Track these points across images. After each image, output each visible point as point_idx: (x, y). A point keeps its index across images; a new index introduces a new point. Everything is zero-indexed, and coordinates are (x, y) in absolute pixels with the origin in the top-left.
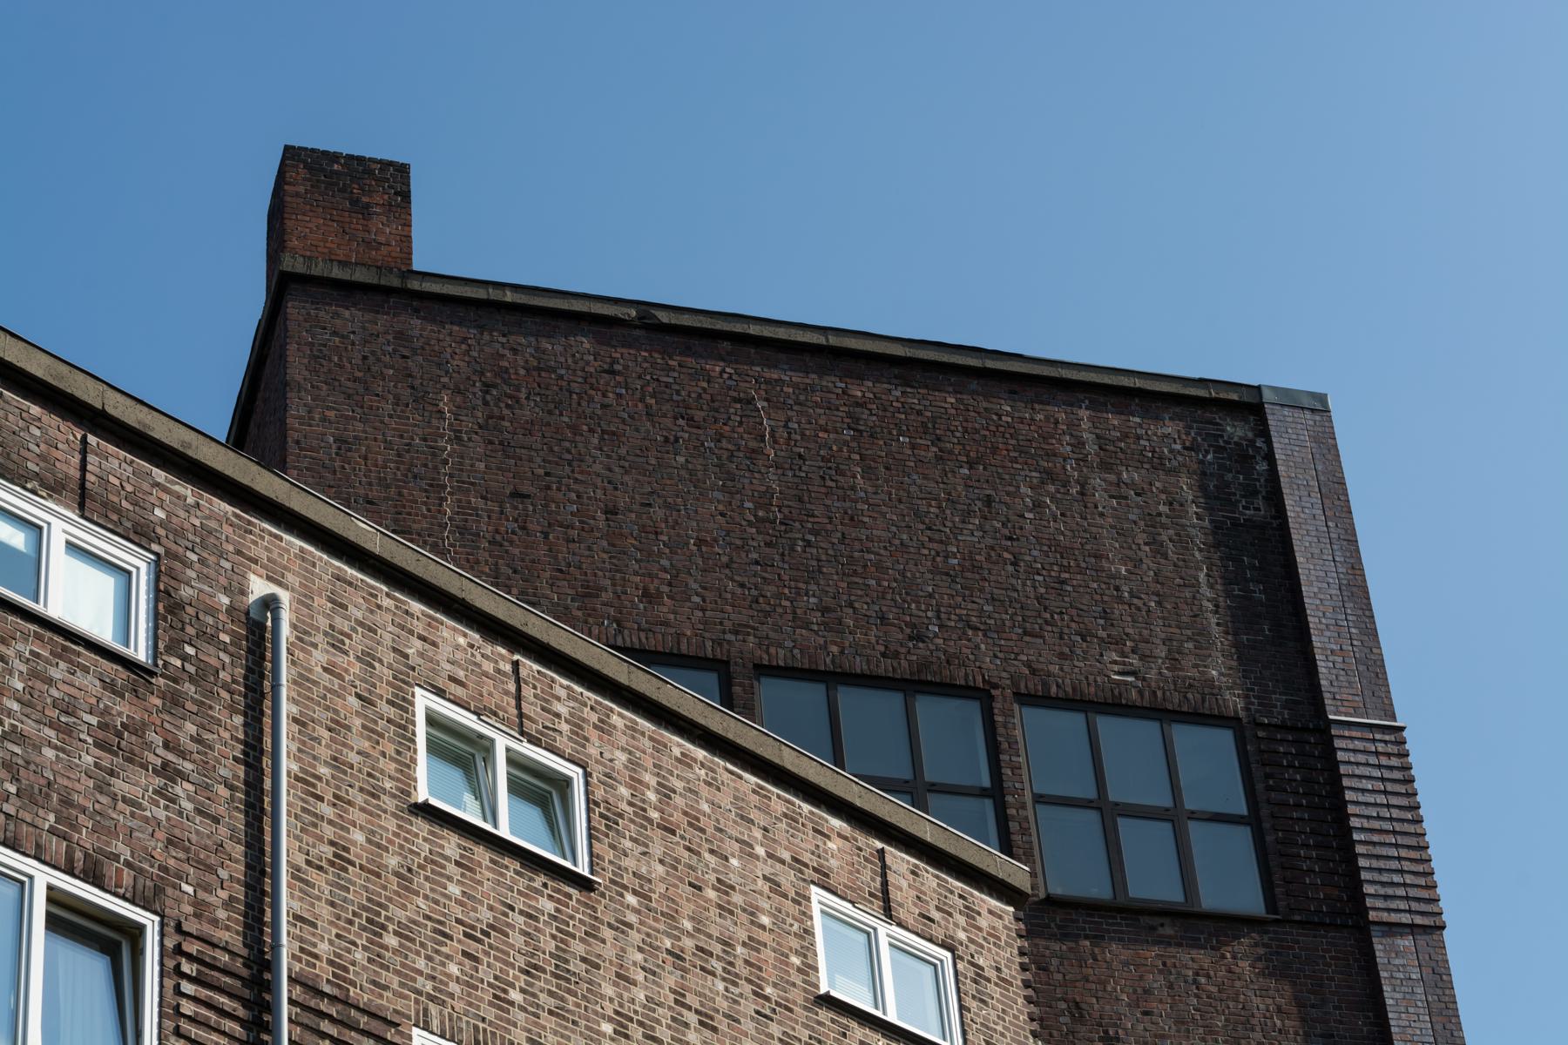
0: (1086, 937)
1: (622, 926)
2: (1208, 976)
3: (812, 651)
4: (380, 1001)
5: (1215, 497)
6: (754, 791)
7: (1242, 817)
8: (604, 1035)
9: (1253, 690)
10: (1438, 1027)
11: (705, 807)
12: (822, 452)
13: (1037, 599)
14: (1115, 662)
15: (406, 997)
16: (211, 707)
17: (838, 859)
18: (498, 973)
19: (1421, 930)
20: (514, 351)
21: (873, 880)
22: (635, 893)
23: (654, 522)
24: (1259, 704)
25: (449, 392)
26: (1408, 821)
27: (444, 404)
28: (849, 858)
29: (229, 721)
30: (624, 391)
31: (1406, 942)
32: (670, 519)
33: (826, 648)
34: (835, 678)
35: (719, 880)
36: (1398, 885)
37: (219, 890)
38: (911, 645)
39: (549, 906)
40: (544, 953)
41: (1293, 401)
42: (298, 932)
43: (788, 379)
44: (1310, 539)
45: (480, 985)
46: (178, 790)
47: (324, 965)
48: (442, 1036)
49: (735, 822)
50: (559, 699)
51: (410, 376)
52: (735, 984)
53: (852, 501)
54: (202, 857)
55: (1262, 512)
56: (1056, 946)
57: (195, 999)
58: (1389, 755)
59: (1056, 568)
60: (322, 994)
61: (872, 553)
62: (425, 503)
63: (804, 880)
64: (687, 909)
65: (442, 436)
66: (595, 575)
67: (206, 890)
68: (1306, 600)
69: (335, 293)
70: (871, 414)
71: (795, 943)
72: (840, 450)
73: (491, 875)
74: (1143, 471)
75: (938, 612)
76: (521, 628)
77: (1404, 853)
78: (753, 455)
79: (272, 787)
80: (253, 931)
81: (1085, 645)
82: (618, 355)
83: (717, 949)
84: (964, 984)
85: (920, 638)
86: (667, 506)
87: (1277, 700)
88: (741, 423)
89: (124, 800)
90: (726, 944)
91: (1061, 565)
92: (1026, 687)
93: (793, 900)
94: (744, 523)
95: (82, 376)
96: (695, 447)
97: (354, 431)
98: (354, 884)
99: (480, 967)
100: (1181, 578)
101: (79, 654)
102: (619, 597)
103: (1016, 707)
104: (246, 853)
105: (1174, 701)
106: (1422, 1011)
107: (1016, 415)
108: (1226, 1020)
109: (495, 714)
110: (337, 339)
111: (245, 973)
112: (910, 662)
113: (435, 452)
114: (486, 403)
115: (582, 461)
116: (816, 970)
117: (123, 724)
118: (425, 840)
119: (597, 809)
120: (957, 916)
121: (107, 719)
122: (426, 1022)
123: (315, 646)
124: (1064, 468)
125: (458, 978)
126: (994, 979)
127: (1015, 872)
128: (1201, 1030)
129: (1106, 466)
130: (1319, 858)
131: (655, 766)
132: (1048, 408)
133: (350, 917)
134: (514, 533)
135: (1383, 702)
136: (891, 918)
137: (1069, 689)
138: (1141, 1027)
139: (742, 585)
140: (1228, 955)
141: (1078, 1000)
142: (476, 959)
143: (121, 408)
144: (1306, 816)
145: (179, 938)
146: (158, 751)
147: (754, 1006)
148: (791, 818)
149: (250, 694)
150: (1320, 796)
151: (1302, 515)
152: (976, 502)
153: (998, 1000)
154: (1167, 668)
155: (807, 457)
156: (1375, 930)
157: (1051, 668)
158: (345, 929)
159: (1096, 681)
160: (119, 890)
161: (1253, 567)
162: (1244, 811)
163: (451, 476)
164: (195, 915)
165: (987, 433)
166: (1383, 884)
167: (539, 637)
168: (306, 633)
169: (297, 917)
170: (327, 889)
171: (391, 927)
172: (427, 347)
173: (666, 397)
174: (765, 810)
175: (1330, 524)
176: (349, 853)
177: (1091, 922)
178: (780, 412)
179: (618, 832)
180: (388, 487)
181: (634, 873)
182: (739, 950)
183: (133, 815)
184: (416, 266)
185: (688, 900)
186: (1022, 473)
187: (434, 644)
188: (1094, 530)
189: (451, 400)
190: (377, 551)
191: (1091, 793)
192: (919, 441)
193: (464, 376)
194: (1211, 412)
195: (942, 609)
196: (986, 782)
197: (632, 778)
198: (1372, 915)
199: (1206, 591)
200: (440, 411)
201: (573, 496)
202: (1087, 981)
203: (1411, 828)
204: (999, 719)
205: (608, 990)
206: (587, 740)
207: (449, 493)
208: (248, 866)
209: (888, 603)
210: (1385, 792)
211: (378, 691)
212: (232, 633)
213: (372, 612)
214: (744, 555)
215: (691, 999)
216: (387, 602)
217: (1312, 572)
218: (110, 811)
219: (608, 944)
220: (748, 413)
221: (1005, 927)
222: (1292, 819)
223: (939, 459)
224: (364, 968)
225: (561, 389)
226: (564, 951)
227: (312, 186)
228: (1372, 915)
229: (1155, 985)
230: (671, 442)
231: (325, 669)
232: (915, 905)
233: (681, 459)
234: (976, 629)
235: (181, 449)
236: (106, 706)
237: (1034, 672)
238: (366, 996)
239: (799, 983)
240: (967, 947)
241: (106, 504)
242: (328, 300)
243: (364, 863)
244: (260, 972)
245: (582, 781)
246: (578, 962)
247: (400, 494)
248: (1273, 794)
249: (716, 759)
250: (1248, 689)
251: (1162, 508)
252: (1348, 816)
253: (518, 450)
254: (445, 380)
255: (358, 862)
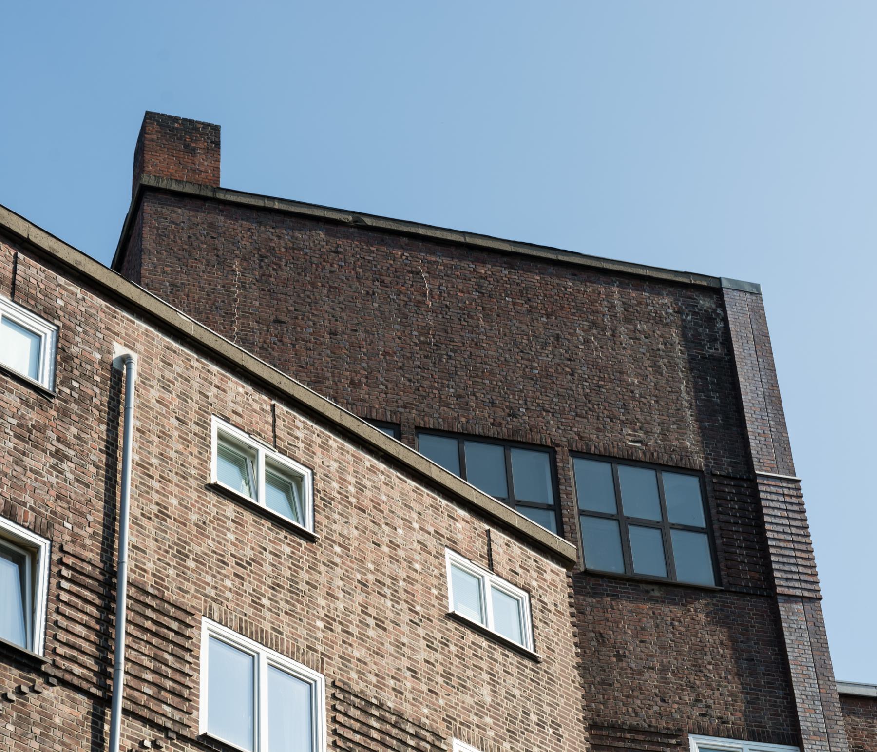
0: (608, 595)
1: (331, 565)
2: (680, 622)
3: (450, 420)
4: (183, 600)
5: (691, 341)
6: (413, 491)
7: (703, 529)
8: (318, 629)
9: (711, 455)
10: (817, 658)
11: (384, 498)
12: (460, 305)
13: (584, 395)
14: (630, 435)
15: (198, 598)
16: (87, 419)
17: (462, 533)
18: (255, 588)
19: (807, 600)
20: (279, 237)
21: (483, 547)
22: (340, 545)
23: (359, 341)
24: (715, 463)
25: (239, 259)
26: (801, 535)
27: (236, 266)
28: (469, 533)
29: (97, 427)
30: (343, 264)
31: (798, 607)
32: (368, 340)
33: (458, 419)
34: (463, 437)
35: (390, 541)
36: (794, 572)
37: (87, 527)
38: (509, 419)
39: (288, 550)
40: (284, 577)
41: (739, 287)
42: (134, 555)
43: (441, 261)
44: (747, 368)
45: (244, 594)
46: (65, 466)
47: (150, 576)
48: (220, 623)
49: (401, 508)
50: (298, 428)
51: (216, 249)
52: (398, 603)
53: (477, 333)
54: (77, 507)
55: (720, 351)
56: (590, 600)
57: (69, 592)
58: (791, 496)
59: (596, 378)
60: (147, 593)
61: (488, 364)
62: (222, 324)
63: (442, 545)
64: (371, 557)
65: (234, 285)
66: (322, 370)
67: (79, 527)
68: (744, 403)
69: (173, 199)
70: (490, 284)
71: (435, 581)
72: (471, 304)
73: (253, 529)
74: (650, 324)
75: (526, 400)
76: (277, 385)
77: (798, 554)
78: (419, 305)
79: (123, 468)
80: (107, 553)
81: (612, 424)
82: (341, 243)
83: (388, 582)
84: (535, 612)
85: (514, 415)
86: (366, 331)
87: (725, 461)
88: (412, 285)
89: (31, 470)
90: (393, 579)
91: (600, 377)
92: (577, 447)
93: (435, 556)
94: (412, 344)
95: (16, 217)
96: (384, 298)
97: (181, 279)
98: (170, 529)
99: (245, 583)
100: (670, 387)
101: (7, 382)
102: (336, 384)
103: (570, 458)
104: (105, 507)
105: (664, 459)
106: (807, 648)
107: (576, 288)
108: (690, 648)
109: (260, 435)
110: (173, 226)
111: (101, 578)
112: (508, 429)
113: (229, 294)
114: (261, 267)
115: (317, 303)
116: (447, 598)
117: (32, 425)
118: (214, 506)
119: (319, 495)
120: (532, 572)
121: (23, 421)
122: (210, 614)
123: (152, 387)
124: (603, 320)
125: (231, 589)
126: (553, 610)
127: (567, 547)
128: (675, 653)
129: (627, 320)
130: (747, 555)
131: (355, 471)
132: (595, 285)
133: (167, 548)
134: (274, 343)
135: (788, 465)
136: (493, 571)
137: (602, 449)
138: (639, 649)
139: (410, 380)
140: (692, 610)
141: (602, 632)
142: (242, 578)
143: (39, 238)
144: (741, 530)
145: (60, 555)
146: (53, 443)
147: (409, 617)
148: (436, 508)
149: (111, 413)
150: (749, 518)
151: (743, 354)
152: (551, 338)
153: (555, 623)
154: (660, 440)
155: (451, 307)
156: (779, 598)
157: (592, 436)
158: (163, 555)
159: (618, 445)
160: (25, 524)
161: (713, 383)
162: (704, 525)
163: (238, 308)
164: (72, 542)
165: (558, 298)
166: (785, 572)
167: (287, 390)
168: (147, 379)
169: (134, 547)
170: (153, 531)
171: (191, 556)
172: (227, 233)
173: (368, 268)
174: (420, 502)
175: (759, 360)
176: (168, 510)
177: (612, 587)
178: (436, 280)
179: (331, 508)
180: (201, 313)
181: (340, 534)
182: (401, 583)
183: (36, 479)
184: (222, 185)
185: (372, 552)
186: (578, 322)
187: (224, 391)
188: (619, 357)
189: (240, 264)
190: (192, 333)
191: (612, 510)
192: (518, 301)
193: (248, 250)
194: (691, 292)
195: (528, 399)
196: (551, 501)
197: (340, 478)
198: (779, 590)
199: (684, 395)
200: (233, 271)
201: (311, 323)
202: (608, 621)
203: (803, 540)
204: (560, 464)
205: (322, 602)
206: (314, 453)
207: (237, 318)
208: (105, 514)
209: (496, 394)
210: (788, 518)
211: (189, 416)
212: (102, 376)
213: (187, 369)
214: (411, 362)
215: (371, 610)
216: (196, 364)
217: (748, 387)
218: (22, 476)
219: (323, 574)
220: (417, 280)
221: (561, 581)
222: (732, 531)
223: (529, 311)
224: (174, 579)
225: (306, 261)
226: (296, 577)
227: (162, 136)
228: (779, 590)
229: (648, 625)
230: (370, 295)
231: (158, 401)
232: (507, 564)
233: (376, 305)
234: (548, 412)
235: (75, 265)
236: (23, 414)
237: (581, 438)
238: (174, 596)
239: (436, 605)
240: (537, 590)
241: (27, 295)
242: (168, 203)
243: (177, 517)
244: (110, 578)
245: (310, 477)
246: (304, 584)
247: (207, 318)
248: (721, 516)
249: (391, 470)
250: (708, 454)
251: (661, 346)
252: (765, 531)
253: (279, 295)
254: (237, 252)
255: (173, 516)
